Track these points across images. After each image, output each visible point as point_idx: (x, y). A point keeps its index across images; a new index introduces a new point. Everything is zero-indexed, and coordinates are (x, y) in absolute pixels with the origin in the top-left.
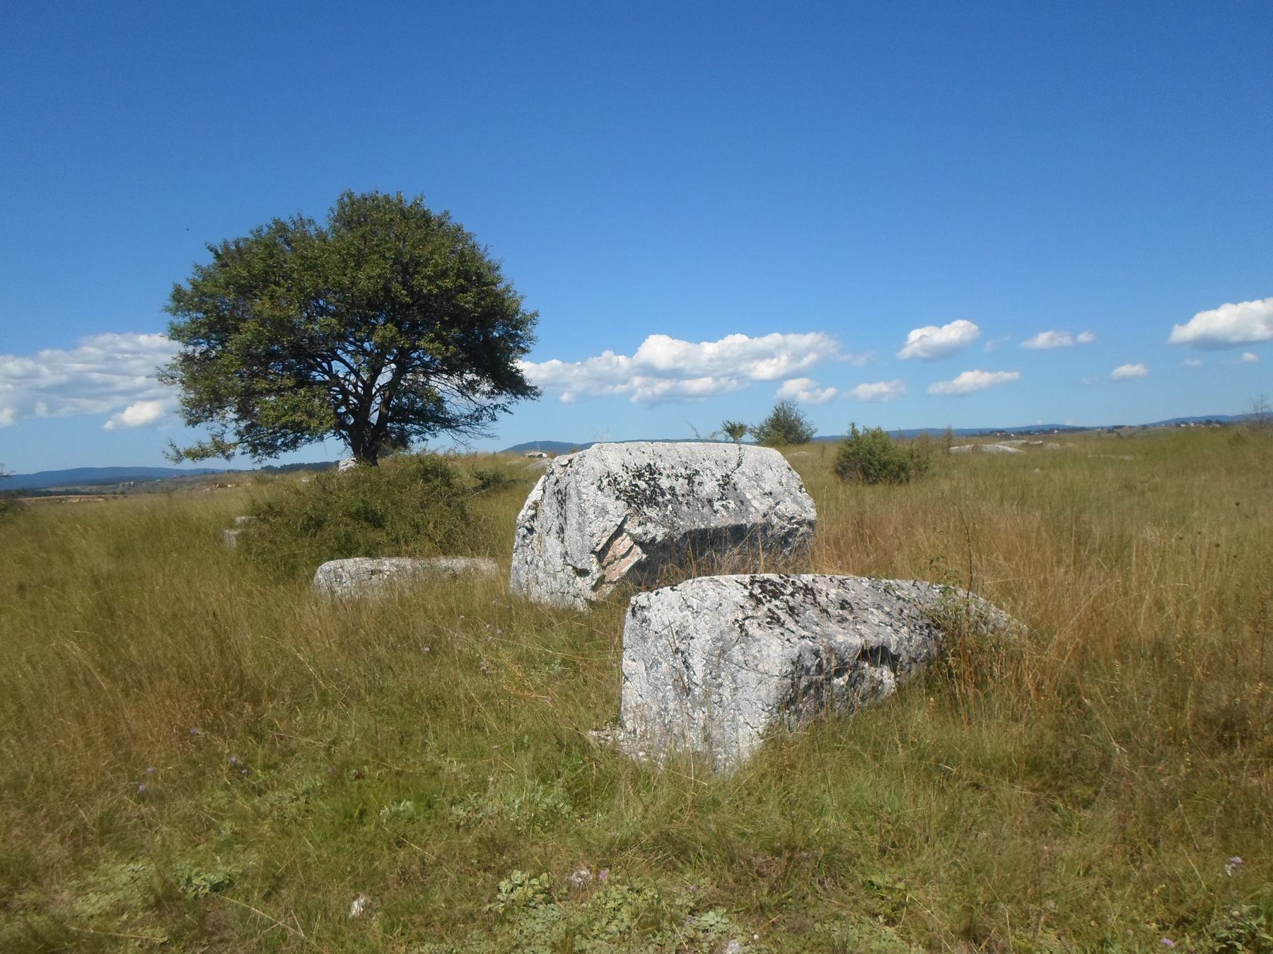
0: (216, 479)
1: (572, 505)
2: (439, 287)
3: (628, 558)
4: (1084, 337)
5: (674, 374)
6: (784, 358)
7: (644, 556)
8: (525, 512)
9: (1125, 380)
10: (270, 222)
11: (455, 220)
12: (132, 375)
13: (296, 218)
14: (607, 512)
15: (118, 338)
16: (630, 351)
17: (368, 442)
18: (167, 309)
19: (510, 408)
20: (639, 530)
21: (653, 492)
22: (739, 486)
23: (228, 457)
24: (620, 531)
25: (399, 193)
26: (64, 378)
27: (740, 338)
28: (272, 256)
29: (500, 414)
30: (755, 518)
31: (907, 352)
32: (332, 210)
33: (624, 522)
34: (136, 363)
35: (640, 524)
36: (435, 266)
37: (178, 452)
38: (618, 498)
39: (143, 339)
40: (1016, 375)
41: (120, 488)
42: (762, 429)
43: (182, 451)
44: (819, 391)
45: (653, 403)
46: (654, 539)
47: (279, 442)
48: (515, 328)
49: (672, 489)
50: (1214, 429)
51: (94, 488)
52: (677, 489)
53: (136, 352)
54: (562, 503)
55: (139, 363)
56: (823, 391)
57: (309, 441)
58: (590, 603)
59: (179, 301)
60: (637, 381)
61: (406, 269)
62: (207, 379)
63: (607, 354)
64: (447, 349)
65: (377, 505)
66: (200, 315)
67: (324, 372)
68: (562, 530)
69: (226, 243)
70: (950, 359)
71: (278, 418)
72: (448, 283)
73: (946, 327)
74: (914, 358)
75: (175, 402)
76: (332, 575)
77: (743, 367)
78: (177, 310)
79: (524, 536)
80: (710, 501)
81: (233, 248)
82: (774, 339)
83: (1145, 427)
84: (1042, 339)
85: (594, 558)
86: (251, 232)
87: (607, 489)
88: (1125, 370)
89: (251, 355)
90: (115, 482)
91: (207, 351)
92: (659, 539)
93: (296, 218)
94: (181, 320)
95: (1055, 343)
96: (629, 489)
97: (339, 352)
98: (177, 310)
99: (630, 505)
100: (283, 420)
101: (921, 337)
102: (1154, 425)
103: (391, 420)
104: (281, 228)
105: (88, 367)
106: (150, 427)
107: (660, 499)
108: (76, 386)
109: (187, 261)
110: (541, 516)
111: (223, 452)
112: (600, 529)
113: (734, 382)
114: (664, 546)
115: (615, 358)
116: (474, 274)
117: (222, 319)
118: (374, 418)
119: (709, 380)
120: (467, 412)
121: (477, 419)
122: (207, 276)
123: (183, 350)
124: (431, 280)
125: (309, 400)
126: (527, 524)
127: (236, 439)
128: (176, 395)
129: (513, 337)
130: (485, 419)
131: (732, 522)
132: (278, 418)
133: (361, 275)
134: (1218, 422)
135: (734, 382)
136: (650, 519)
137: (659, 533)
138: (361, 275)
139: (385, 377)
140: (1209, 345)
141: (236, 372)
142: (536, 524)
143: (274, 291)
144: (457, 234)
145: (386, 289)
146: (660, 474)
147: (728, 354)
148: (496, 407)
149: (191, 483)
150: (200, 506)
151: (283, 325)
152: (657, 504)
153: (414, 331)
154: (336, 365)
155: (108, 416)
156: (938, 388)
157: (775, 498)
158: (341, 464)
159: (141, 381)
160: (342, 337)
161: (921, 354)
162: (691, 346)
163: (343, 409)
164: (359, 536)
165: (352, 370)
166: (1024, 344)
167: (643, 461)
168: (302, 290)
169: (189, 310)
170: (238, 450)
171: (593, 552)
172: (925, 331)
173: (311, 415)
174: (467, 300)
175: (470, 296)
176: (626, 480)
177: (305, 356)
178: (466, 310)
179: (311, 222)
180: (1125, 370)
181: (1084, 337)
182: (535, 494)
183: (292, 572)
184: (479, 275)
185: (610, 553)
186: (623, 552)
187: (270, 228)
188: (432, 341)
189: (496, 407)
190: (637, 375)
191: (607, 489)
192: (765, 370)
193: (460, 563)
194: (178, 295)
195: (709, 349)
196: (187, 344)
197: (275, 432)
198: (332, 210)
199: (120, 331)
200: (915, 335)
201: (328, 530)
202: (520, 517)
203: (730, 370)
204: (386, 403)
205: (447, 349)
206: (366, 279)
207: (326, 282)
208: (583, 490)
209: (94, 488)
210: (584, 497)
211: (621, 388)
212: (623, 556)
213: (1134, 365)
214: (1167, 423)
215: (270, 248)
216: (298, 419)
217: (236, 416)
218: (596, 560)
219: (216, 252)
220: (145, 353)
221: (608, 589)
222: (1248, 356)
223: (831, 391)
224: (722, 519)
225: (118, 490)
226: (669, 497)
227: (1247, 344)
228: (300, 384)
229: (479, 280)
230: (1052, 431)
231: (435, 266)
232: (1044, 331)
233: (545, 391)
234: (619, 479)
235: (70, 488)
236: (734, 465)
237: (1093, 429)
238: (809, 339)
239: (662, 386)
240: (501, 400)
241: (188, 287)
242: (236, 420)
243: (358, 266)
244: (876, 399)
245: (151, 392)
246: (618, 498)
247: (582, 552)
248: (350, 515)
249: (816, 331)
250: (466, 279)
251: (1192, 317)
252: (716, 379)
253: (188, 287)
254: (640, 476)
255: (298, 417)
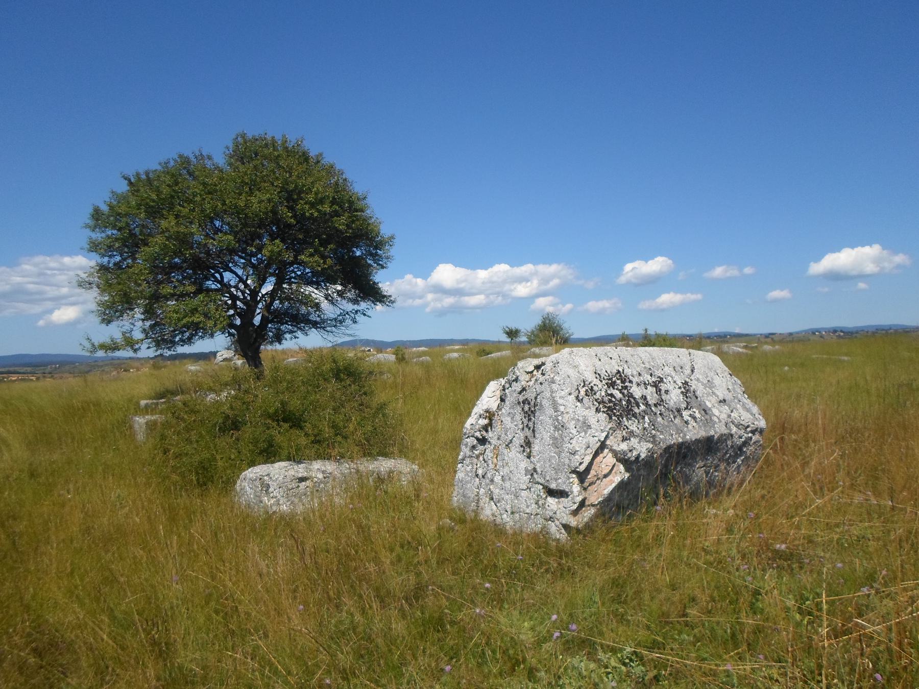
0: (123, 366)
1: (544, 419)
2: (319, 211)
3: (610, 477)
4: (748, 270)
5: (457, 292)
6: (535, 282)
7: (627, 475)
8: (474, 421)
9: (775, 301)
10: (176, 157)
11: (327, 159)
12: (58, 286)
13: (197, 153)
14: (589, 427)
15: (48, 258)
16: (425, 275)
17: (249, 342)
18: (87, 226)
19: (369, 313)
20: (624, 446)
21: (629, 402)
22: (698, 393)
23: (135, 351)
24: (603, 446)
25: (284, 136)
26: (7, 288)
27: (502, 268)
28: (177, 184)
29: (360, 318)
30: (719, 429)
31: (623, 279)
32: (227, 148)
33: (607, 437)
34: (62, 278)
35: (624, 439)
36: (316, 194)
37: (93, 345)
38: (598, 410)
39: (67, 260)
40: (699, 296)
41: (49, 369)
42: (533, 332)
43: (96, 344)
44: (560, 306)
45: (442, 313)
46: (639, 456)
47: (177, 339)
48: (376, 248)
49: (644, 398)
50: (839, 336)
51: (29, 369)
52: (648, 397)
53: (63, 269)
54: (530, 414)
55: (63, 277)
56: (564, 305)
57: (202, 337)
58: (566, 527)
59: (97, 220)
60: (430, 297)
61: (291, 196)
62: (119, 284)
63: (409, 277)
64: (325, 263)
65: (295, 404)
66: (115, 232)
67: (216, 280)
68: (528, 443)
69: (138, 174)
70: (653, 284)
71: (179, 320)
72: (326, 208)
73: (650, 262)
74: (629, 283)
75: (93, 306)
76: (258, 483)
77: (507, 287)
78: (95, 227)
79: (474, 447)
80: (679, 411)
81: (144, 177)
82: (528, 268)
83: (791, 334)
84: (719, 271)
85: (574, 479)
86: (160, 164)
87: (586, 399)
88: (776, 294)
89: (157, 267)
90: (45, 365)
91: (120, 261)
92: (643, 456)
93: (197, 153)
94: (98, 236)
95: (728, 274)
96: (606, 399)
97: (230, 265)
98: (95, 227)
99: (611, 418)
100: (184, 321)
101: (635, 269)
102: (797, 333)
103: (271, 321)
104: (185, 161)
105: (26, 279)
106: (72, 325)
107: (636, 410)
108: (17, 294)
109: (106, 186)
110: (498, 428)
111: (132, 347)
112: (581, 445)
113: (500, 298)
114: (649, 463)
115: (414, 280)
116: (348, 204)
117: (132, 235)
118: (257, 320)
119: (482, 297)
120: (333, 316)
121: (341, 322)
122: (122, 199)
123: (99, 261)
124: (312, 205)
125: (206, 305)
126: (478, 434)
127: (142, 336)
128: (92, 298)
129: (374, 256)
130: (348, 322)
131: (702, 434)
132: (179, 320)
133: (253, 200)
134: (842, 331)
135: (500, 298)
136: (632, 433)
137: (642, 449)
138: (253, 200)
139: (268, 288)
140: (835, 277)
141: (145, 280)
142: (490, 435)
143: (180, 211)
144: (330, 170)
145: (274, 212)
146: (631, 382)
147: (495, 279)
148: (356, 312)
149: (102, 366)
150: (110, 390)
151: (184, 240)
152: (635, 415)
153: (297, 247)
154: (227, 276)
155: (39, 316)
156: (645, 305)
157: (729, 406)
158: (218, 354)
159: (65, 290)
160: (232, 252)
161: (634, 280)
162: (469, 272)
163: (231, 312)
164: (279, 439)
165: (241, 280)
166: (706, 275)
167: (613, 367)
168: (203, 211)
169: (106, 227)
170: (144, 346)
171: (574, 472)
172: (636, 264)
173: (206, 315)
174: (341, 223)
175: (343, 219)
176: (601, 392)
177: (202, 267)
178: (341, 231)
179: (210, 158)
180: (776, 294)
181: (748, 270)
182: (489, 399)
183: (211, 478)
184: (351, 203)
185: (592, 472)
186: (606, 471)
187: (175, 161)
188: (311, 255)
189: (356, 312)
190: (431, 292)
191: (586, 399)
192: (522, 290)
193: (384, 465)
194: (97, 214)
195: (482, 274)
196: (103, 256)
197: (175, 331)
198: (227, 148)
199: (50, 254)
200: (629, 267)
201: (247, 432)
202: (468, 425)
203: (497, 289)
204: (268, 307)
205: (325, 263)
206: (259, 202)
207: (224, 204)
208: (560, 401)
209: (29, 369)
210: (562, 408)
211: (418, 302)
212: (605, 476)
213: (782, 290)
214: (806, 331)
215: (175, 178)
216: (196, 320)
217: (143, 317)
218: (576, 480)
219: (129, 180)
220: (68, 270)
221: (588, 513)
222: (862, 285)
223: (569, 306)
224: (694, 432)
225: (47, 371)
226: (643, 407)
227: (862, 277)
228: (199, 291)
229: (350, 207)
230: (725, 336)
231: (316, 194)
232: (719, 266)
233: (398, 299)
234: (595, 388)
235: (12, 369)
236: (688, 371)
237: (755, 335)
238: (553, 268)
239: (449, 301)
240: (363, 305)
241: (105, 208)
242: (143, 320)
243: (251, 193)
244: (601, 312)
245: (72, 299)
246: (598, 410)
247: (557, 470)
248: (270, 416)
249: (559, 263)
250: (340, 206)
251: (823, 257)
252: (487, 296)
253: (105, 208)
254: (612, 385)
255: (197, 318)
